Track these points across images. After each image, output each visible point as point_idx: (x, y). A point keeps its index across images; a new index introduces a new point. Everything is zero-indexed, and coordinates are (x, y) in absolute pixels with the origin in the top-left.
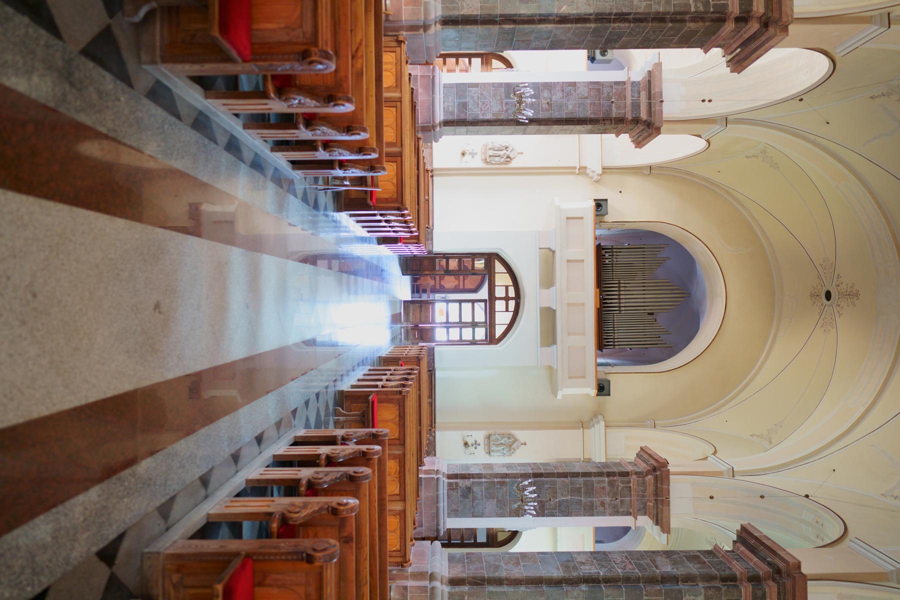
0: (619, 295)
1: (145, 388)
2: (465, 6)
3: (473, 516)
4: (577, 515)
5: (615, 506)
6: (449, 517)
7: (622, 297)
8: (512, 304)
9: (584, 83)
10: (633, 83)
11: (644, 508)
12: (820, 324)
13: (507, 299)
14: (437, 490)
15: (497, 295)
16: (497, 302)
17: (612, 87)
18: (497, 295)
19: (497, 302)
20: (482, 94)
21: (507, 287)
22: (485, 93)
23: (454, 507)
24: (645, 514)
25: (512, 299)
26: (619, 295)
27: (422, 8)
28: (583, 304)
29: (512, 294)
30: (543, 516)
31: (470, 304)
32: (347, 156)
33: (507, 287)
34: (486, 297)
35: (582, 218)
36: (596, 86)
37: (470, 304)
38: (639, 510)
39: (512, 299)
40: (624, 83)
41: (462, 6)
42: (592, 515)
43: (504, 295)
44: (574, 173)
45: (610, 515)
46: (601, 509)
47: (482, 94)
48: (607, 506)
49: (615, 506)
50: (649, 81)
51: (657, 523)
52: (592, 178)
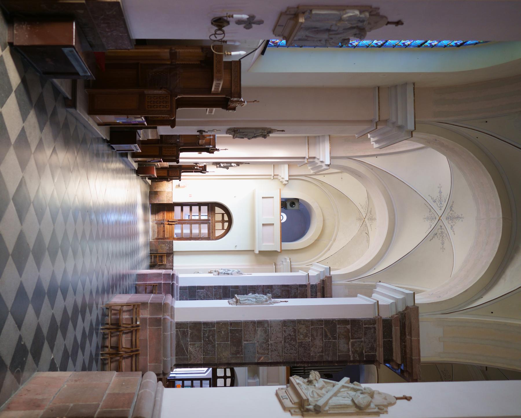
0: (304, 370)
2: (192, 357)
7: (306, 368)
8: (226, 225)
9: (278, 286)
10: (312, 286)
15: (218, 375)
16: (218, 380)
17: (297, 289)
19: (218, 380)
20: (207, 294)
21: (223, 214)
22: (209, 293)
25: (229, 377)
26: (304, 370)
27: (162, 365)
29: (226, 218)
34: (210, 376)
36: (286, 288)
39: (229, 377)
40: (305, 286)
41: (190, 357)
44: (270, 179)
47: (207, 294)
50: (323, 288)
52: (282, 182)
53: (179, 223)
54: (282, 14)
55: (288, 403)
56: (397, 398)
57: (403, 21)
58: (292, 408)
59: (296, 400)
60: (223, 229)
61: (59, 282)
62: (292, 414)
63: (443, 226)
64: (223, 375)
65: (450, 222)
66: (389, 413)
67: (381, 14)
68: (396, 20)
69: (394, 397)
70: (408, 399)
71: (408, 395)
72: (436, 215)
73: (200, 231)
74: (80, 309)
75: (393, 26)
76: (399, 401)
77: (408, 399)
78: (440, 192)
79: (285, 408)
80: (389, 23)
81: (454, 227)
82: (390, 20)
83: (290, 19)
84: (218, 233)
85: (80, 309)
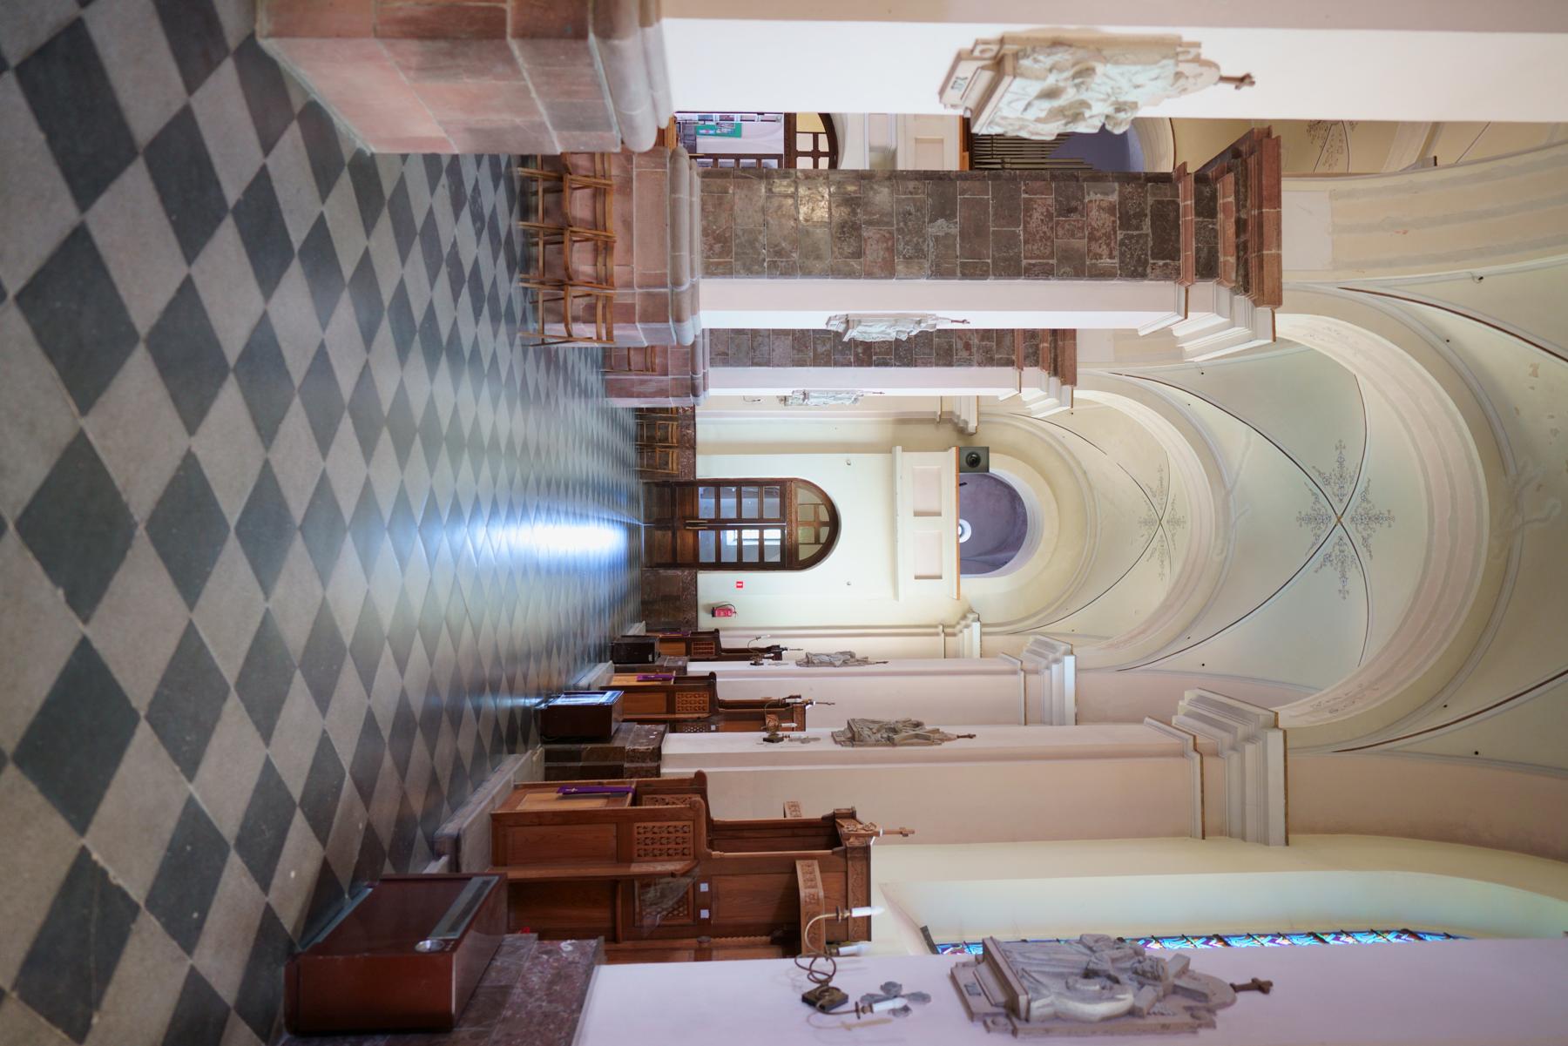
1: (215, 503)
3: (754, 364)
4: (925, 364)
5: (987, 350)
6: (712, 364)
11: (1035, 353)
12: (1323, 160)
13: (815, 154)
14: (694, 372)
15: (800, 148)
18: (800, 148)
19: (799, 159)
21: (816, 135)
23: (722, 348)
24: (1036, 364)
25: (824, 154)
28: (941, 141)
29: (824, 146)
30: (869, 365)
31: (744, 516)
32: (553, 433)
33: (816, 135)
35: (917, 514)
37: (744, 516)
38: (1026, 357)
39: (824, 154)
42: (950, 364)
43: (810, 148)
45: (980, 365)
46: (965, 354)
48: (974, 350)
49: (987, 350)
51: (1056, 373)
53: (710, 528)
54: (959, 58)
55: (980, 1004)
56: (1237, 989)
57: (1256, 77)
58: (987, 1014)
59: (1000, 997)
60: (817, 541)
61: (386, 628)
62: (988, 1030)
63: (1346, 539)
64: (810, 148)
65: (1360, 528)
66: (1218, 1025)
67: (1203, 57)
68: (1240, 74)
69: (1232, 985)
70: (1262, 987)
71: (1262, 978)
72: (1330, 511)
73: (761, 503)
74: (417, 337)
75: (1230, 87)
76: (1242, 997)
77: (1262, 987)
78: (1341, 463)
79: (972, 1015)
80: (1224, 79)
81: (1370, 541)
82: (1225, 73)
83: (983, 68)
84: (804, 553)
85: (417, 337)
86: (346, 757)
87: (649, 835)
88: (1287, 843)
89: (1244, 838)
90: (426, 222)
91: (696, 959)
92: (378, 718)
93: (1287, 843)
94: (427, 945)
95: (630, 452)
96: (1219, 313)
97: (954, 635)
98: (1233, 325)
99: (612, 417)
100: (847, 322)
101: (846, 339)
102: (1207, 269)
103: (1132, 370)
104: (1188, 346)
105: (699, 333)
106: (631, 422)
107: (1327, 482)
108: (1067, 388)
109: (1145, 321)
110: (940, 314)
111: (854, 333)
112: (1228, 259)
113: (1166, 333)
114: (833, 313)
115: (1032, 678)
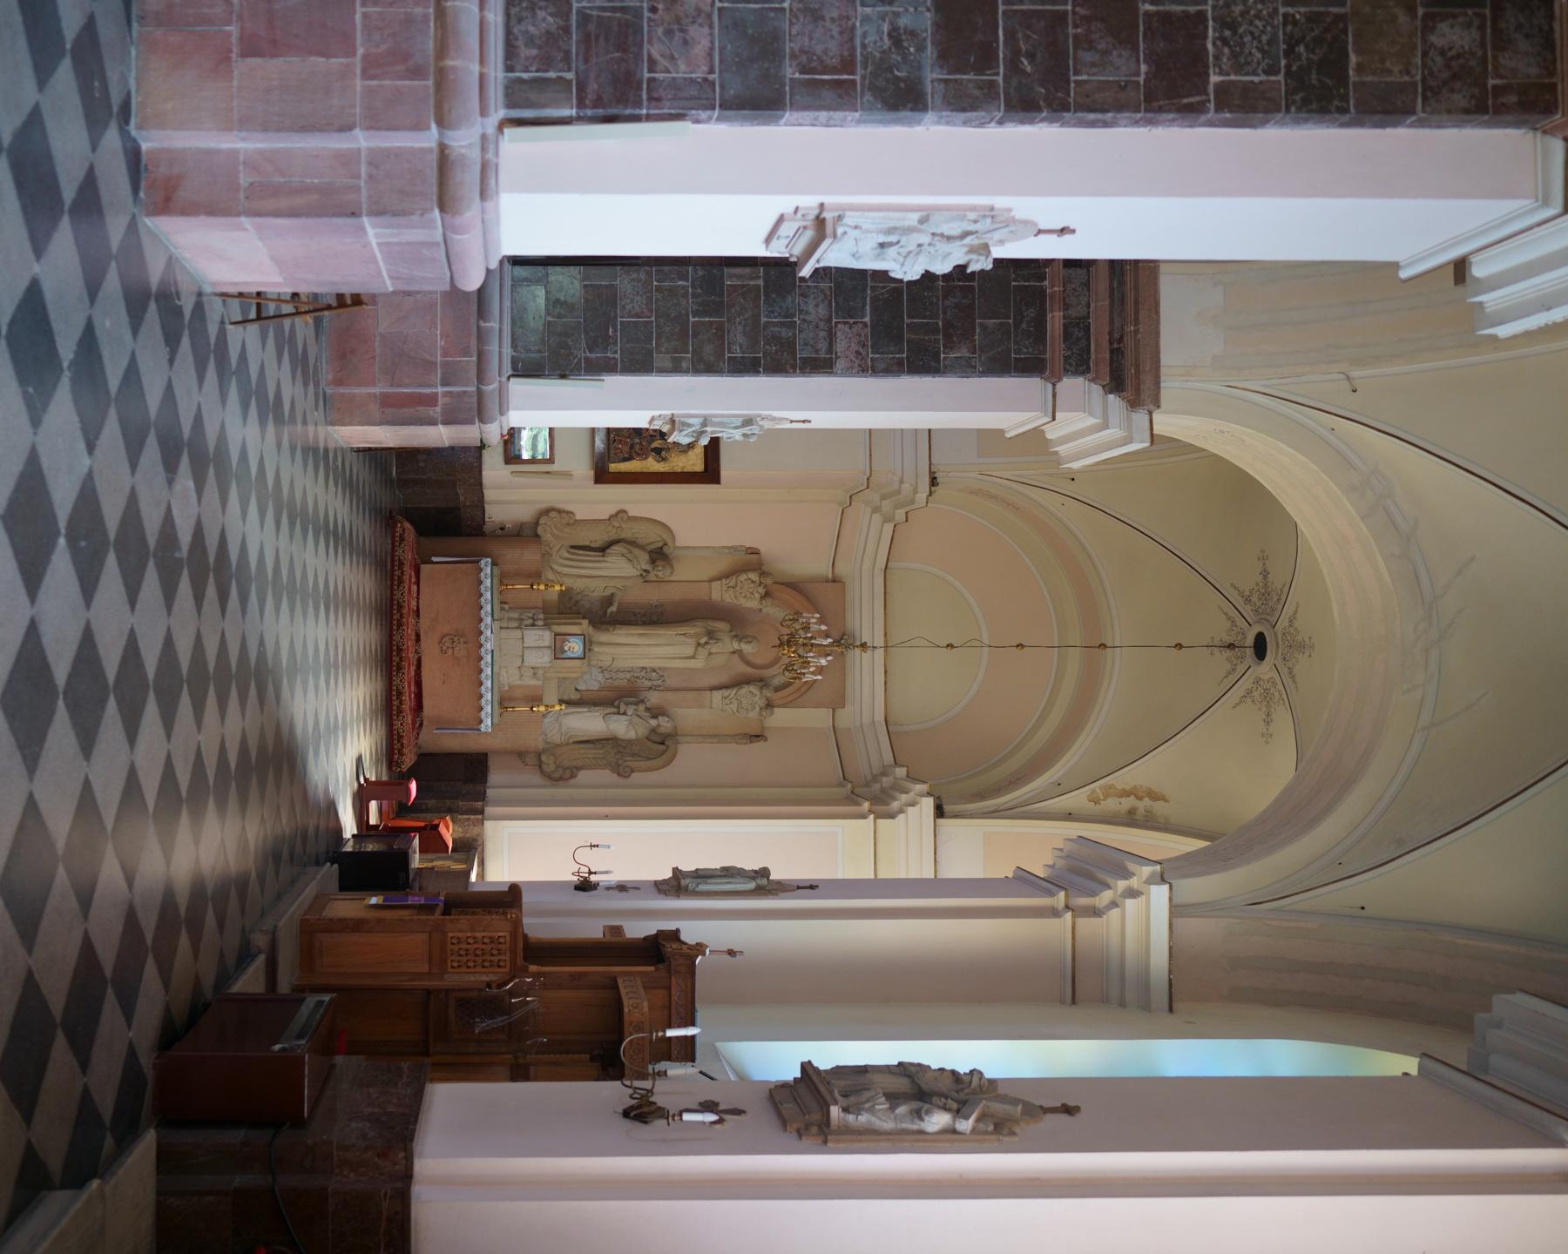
77: (1069, 1110)
78: (1265, 574)
86: (57, 1004)
87: (464, 946)
88: (1171, 1010)
89: (1122, 1004)
90: (178, 342)
91: (514, 1079)
92: (140, 915)
93: (1171, 1010)
94: (277, 1047)
95: (364, 529)
96: (1091, 414)
97: (1096, 912)
98: (1105, 425)
99: (319, 456)
100: (820, 222)
101: (670, 440)
102: (1079, 365)
103: (1007, 474)
104: (1062, 449)
105: (494, 265)
106: (361, 472)
107: (1248, 600)
108: (1140, 418)
109: (1013, 421)
110: (1024, 207)
111: (834, 255)
112: (1099, 349)
113: (1037, 433)
114: (657, 413)
115: (1082, 922)
